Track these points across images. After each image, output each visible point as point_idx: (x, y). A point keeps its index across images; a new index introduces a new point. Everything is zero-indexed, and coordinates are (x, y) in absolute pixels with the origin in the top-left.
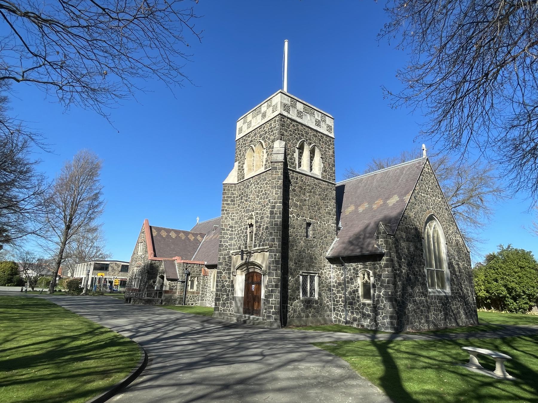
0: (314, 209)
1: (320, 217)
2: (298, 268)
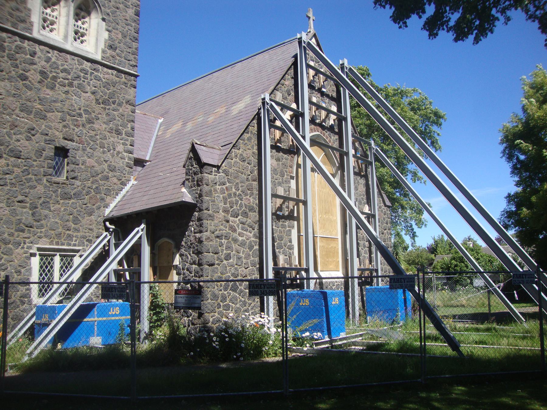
0: (77, 120)
1: (92, 137)
2: (27, 240)
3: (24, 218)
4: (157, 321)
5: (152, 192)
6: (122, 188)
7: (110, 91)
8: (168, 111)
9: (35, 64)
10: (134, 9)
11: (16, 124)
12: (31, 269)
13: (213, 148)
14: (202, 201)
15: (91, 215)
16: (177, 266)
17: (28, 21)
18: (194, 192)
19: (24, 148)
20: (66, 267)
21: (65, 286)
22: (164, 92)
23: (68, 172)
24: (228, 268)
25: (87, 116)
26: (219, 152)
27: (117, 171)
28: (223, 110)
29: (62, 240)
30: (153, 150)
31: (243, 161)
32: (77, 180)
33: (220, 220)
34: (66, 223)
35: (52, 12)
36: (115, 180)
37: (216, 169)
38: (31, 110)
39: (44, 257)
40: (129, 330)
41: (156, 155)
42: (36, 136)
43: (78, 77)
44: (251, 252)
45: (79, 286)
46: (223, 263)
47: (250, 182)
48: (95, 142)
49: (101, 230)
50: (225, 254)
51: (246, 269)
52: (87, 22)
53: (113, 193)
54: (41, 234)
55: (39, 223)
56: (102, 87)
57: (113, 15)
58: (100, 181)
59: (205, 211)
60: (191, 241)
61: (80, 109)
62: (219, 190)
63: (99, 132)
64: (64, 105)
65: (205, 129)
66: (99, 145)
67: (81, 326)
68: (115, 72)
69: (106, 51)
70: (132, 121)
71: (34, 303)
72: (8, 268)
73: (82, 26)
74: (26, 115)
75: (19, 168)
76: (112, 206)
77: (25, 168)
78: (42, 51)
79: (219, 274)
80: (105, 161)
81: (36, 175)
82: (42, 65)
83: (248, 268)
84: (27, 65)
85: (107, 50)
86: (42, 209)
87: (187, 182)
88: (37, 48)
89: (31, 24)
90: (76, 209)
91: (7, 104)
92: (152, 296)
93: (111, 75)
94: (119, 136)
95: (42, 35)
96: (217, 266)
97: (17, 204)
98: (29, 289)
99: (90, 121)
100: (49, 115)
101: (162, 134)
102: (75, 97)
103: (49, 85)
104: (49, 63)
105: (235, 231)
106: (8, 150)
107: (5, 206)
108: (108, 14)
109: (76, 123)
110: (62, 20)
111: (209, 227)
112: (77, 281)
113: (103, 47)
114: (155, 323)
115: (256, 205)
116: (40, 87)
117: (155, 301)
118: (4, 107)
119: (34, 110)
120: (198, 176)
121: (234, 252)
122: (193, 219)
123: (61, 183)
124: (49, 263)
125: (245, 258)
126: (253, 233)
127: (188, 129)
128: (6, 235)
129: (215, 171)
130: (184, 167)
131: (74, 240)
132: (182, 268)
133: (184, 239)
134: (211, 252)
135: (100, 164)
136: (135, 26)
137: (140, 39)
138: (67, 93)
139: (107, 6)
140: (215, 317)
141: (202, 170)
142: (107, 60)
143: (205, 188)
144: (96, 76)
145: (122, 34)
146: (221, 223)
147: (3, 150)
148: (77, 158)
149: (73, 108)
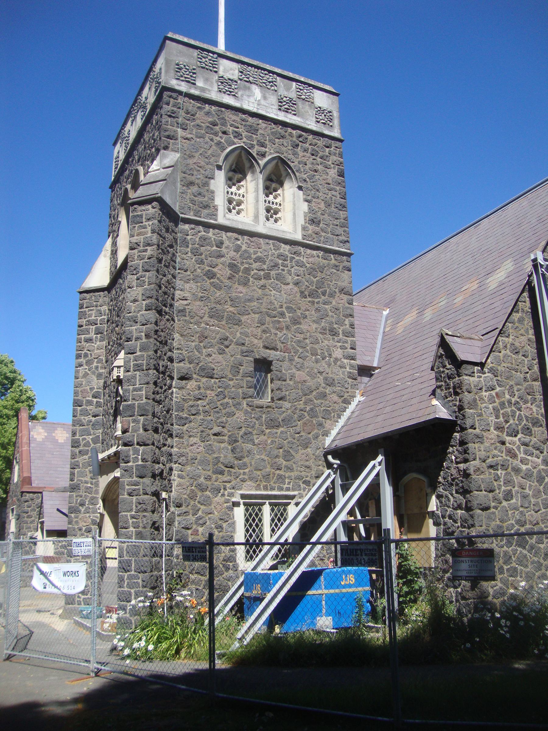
0: (279, 322)
1: (299, 341)
2: (228, 485)
3: (222, 455)
4: (407, 594)
5: (388, 409)
6: (346, 408)
7: (317, 278)
8: (395, 299)
9: (223, 256)
10: (336, 168)
11: (206, 334)
12: (234, 523)
13: (471, 339)
14: (464, 416)
15: (307, 447)
16: (433, 512)
17: (211, 206)
18: (451, 404)
19: (216, 364)
20: (279, 520)
21: (277, 547)
22: (385, 275)
23: (272, 391)
24: (510, 512)
25: (291, 315)
26: (479, 344)
27: (337, 385)
28: (475, 286)
29: (272, 483)
30: (381, 353)
31: (516, 353)
32: (285, 401)
33: (493, 441)
34: (275, 460)
35: (238, 190)
36: (335, 398)
37: (479, 368)
38: (222, 314)
39: (250, 506)
40: (370, 607)
41: (386, 358)
42: (230, 347)
43: (276, 265)
44: (542, 487)
45: (297, 547)
46: (502, 505)
47: (529, 383)
48: (305, 348)
49: (321, 467)
50: (504, 491)
51: (536, 512)
52: (279, 195)
53: (334, 416)
54: (244, 476)
55: (241, 461)
56: (306, 274)
57: (311, 181)
58: (315, 400)
59: (470, 431)
60: (452, 475)
61: (281, 307)
62: (486, 399)
63: (308, 334)
64: (262, 303)
65: (453, 315)
66: (310, 352)
67: (304, 600)
68: (321, 253)
69: (307, 227)
70: (350, 315)
71: (240, 569)
72: (206, 522)
73: (275, 201)
74: (216, 321)
75: (212, 390)
76: (334, 433)
77: (219, 390)
78: (229, 238)
79: (498, 523)
80: (319, 372)
81: (233, 398)
82: (232, 256)
83: (539, 511)
84: (213, 259)
85: (308, 225)
86: (243, 443)
87: (438, 391)
88: (224, 236)
89: (216, 208)
90: (287, 441)
91: (194, 310)
92: (399, 558)
93: (317, 258)
94: (334, 337)
95: (229, 219)
96: (494, 510)
97: (213, 437)
98: (234, 551)
99: (296, 322)
100: (244, 318)
101: (390, 330)
102: (274, 292)
103: (241, 280)
104: (240, 253)
105: (514, 456)
106: (198, 368)
107: (199, 441)
108: (305, 181)
109: (277, 326)
110: (250, 198)
111: (477, 453)
112: (294, 538)
113: (303, 223)
114: (406, 597)
115: (542, 415)
116: (230, 284)
117: (405, 565)
118: (191, 314)
119: (226, 314)
120: (454, 380)
121: (516, 488)
122: (453, 444)
123: (265, 406)
124: (257, 515)
125: (534, 496)
126: (541, 458)
127: (428, 319)
128: (202, 479)
129: (478, 372)
130: (432, 369)
131: (287, 483)
132: (442, 515)
133: (442, 473)
134: (483, 489)
135: (313, 377)
136: (340, 190)
137: (348, 206)
138: (263, 288)
139: (302, 170)
140: (497, 587)
141: (460, 371)
142: (310, 239)
143: (467, 397)
144: (297, 262)
145: (325, 203)
146: (493, 446)
147: (192, 368)
148: (283, 371)
149: (273, 307)
